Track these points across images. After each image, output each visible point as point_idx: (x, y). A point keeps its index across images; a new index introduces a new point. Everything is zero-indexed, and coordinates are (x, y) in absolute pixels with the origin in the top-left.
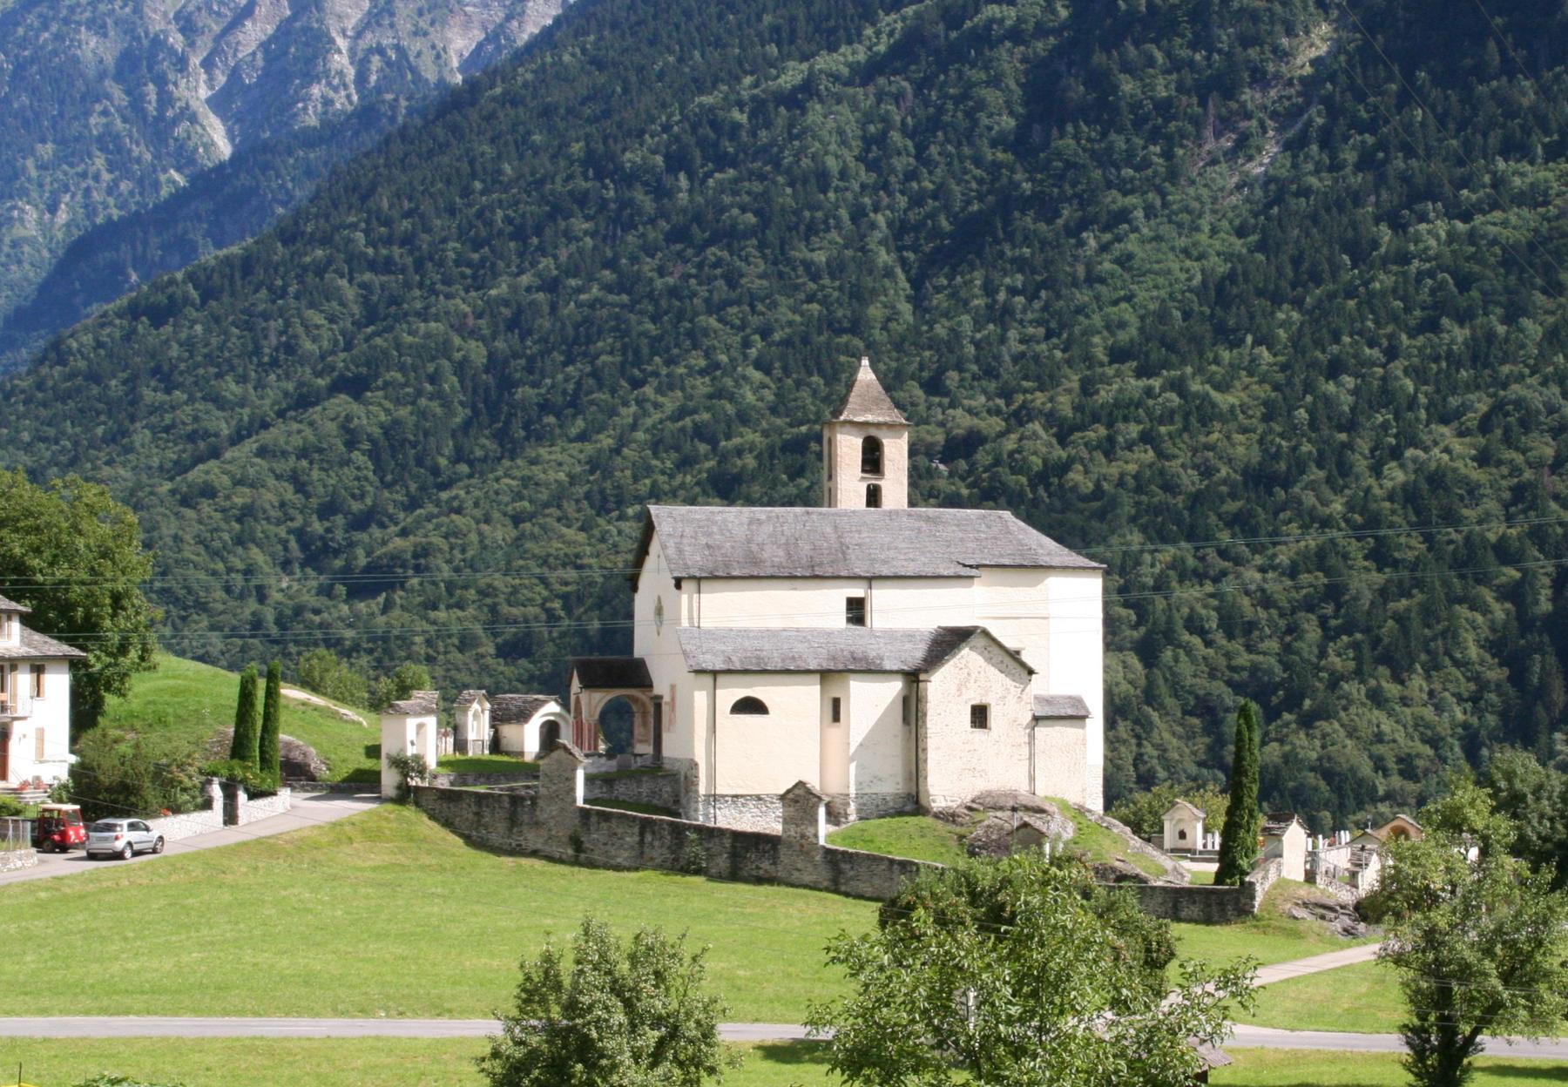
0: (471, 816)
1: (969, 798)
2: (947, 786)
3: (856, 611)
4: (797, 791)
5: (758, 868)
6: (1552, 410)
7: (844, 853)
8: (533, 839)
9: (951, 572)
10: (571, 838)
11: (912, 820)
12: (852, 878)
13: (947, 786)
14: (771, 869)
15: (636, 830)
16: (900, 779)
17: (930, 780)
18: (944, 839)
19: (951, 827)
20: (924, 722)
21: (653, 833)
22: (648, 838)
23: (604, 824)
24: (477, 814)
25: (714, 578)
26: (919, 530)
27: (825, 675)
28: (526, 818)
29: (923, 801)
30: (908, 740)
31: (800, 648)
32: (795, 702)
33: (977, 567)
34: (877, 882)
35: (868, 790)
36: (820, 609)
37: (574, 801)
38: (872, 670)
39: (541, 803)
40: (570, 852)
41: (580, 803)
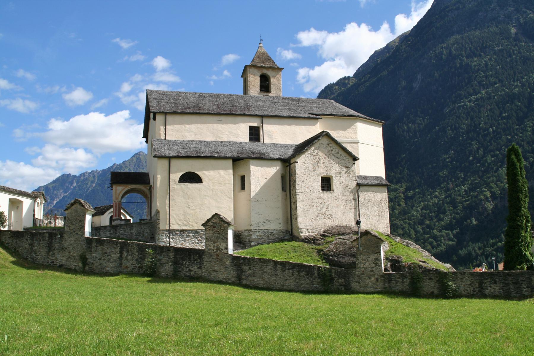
0: (27, 246)
1: (322, 230)
2: (308, 223)
3: (255, 134)
4: (214, 220)
5: (190, 271)
6: (401, 225)
7: (245, 258)
8: (60, 258)
9: (306, 116)
10: (81, 256)
11: (289, 245)
12: (249, 275)
13: (308, 223)
14: (199, 271)
15: (118, 250)
16: (281, 221)
17: (299, 220)
18: (309, 252)
19: (314, 246)
20: (295, 187)
21: (128, 251)
22: (125, 254)
23: (100, 248)
24: (31, 245)
25: (174, 113)
26: (288, 103)
27: (237, 161)
28: (57, 246)
29: (295, 233)
30: (286, 199)
31: (220, 148)
32: (218, 179)
33: (320, 115)
34: (266, 276)
35: (262, 228)
36: (236, 132)
37: (84, 234)
38: (263, 158)
39: (65, 236)
40: (80, 265)
41: (87, 235)
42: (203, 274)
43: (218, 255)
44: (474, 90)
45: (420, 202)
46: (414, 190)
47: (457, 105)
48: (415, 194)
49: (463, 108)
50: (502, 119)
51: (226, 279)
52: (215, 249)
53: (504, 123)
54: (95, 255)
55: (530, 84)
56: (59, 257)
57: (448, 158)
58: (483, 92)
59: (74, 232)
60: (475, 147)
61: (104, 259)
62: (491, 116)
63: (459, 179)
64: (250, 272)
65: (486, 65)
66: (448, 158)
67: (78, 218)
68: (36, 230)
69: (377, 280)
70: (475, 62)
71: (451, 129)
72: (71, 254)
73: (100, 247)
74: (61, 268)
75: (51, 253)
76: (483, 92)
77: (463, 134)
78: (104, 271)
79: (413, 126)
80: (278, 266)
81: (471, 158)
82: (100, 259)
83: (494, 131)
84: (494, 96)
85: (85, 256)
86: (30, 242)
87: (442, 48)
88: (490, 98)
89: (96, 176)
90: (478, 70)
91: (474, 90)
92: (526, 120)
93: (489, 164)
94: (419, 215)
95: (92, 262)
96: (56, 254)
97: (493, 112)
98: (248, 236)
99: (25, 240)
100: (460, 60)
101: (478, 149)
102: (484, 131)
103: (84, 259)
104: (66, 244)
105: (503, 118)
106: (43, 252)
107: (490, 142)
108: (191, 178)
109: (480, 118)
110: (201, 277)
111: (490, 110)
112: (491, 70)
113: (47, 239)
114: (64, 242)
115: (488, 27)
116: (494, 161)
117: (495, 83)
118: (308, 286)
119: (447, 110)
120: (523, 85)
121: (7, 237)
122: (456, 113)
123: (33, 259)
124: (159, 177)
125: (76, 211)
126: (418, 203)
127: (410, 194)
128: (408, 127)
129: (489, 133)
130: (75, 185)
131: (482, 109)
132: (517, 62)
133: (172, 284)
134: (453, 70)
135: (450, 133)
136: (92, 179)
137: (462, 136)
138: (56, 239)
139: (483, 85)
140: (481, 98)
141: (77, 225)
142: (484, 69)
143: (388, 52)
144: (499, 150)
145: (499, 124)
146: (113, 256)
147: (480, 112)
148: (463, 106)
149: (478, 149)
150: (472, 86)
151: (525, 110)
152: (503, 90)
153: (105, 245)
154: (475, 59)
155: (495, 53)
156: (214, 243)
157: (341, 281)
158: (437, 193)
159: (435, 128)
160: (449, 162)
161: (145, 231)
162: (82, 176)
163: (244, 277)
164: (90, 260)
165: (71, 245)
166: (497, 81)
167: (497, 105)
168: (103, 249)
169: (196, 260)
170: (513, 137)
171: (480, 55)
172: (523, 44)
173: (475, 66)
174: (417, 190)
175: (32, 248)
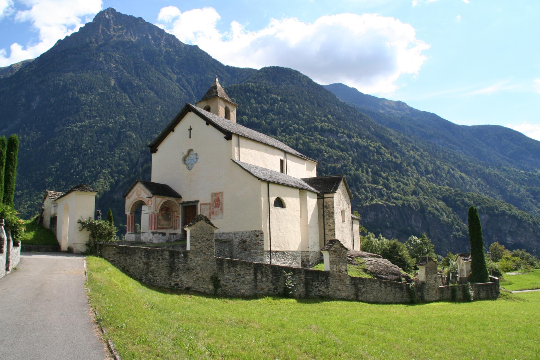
0: (142, 265)
5: (319, 291)
8: (186, 280)
10: (212, 278)
12: (364, 293)
15: (252, 271)
21: (262, 273)
22: (259, 276)
34: (375, 293)
40: (211, 287)
42: (330, 293)
43: (340, 276)
44: (80, 118)
45: (27, 201)
46: (22, 190)
47: (65, 127)
48: (23, 194)
49: (70, 131)
50: (98, 145)
51: (347, 296)
52: (338, 271)
53: (99, 148)
54: (227, 276)
55: (120, 122)
56: (183, 278)
57: (54, 168)
58: (87, 121)
59: (201, 251)
60: (76, 162)
61: (238, 281)
62: (91, 141)
63: (61, 186)
64: (364, 290)
65: (91, 102)
66: (54, 168)
67: (205, 236)
68: (122, 244)
69: (437, 292)
70: (83, 98)
71: (59, 146)
72: (200, 275)
73: (232, 268)
75: (173, 274)
76: (87, 121)
77: (68, 151)
78: (239, 293)
79: (28, 138)
80: (382, 284)
81: (72, 171)
82: (233, 281)
83: (92, 153)
84: (94, 126)
85: (217, 278)
86: (145, 260)
87: (60, 80)
88: (91, 127)
90: (85, 104)
91: (80, 118)
92: (115, 149)
93: (86, 177)
94: (25, 212)
95: (225, 284)
96: (180, 275)
97: (93, 138)
98: (306, 256)
99: (137, 258)
100: (73, 93)
101: (78, 165)
102: (85, 151)
103: (215, 281)
104: (192, 265)
105: (100, 144)
106: (164, 273)
107: (88, 160)
108: (279, 203)
109: (83, 141)
110: (328, 295)
111: (90, 136)
112: (95, 106)
113: (168, 257)
114: (189, 262)
115: (96, 73)
116: (90, 176)
117: (96, 117)
118: (400, 299)
119: (57, 130)
120: (115, 122)
121: (111, 253)
122: (64, 133)
123: (149, 280)
124: (262, 199)
125: (202, 228)
126: (25, 202)
127: (18, 193)
128: (23, 138)
129: (88, 154)
131: (85, 134)
132: (113, 104)
133: (235, 300)
134: (66, 99)
135: (58, 148)
137: (67, 153)
138: (179, 258)
139: (87, 116)
140: (85, 126)
141: (204, 244)
142: (90, 104)
143: (12, 72)
144: (95, 168)
145: (96, 148)
146: (247, 277)
147: (83, 136)
148: (70, 129)
149: (78, 165)
150: (79, 115)
151: (115, 141)
152: (101, 123)
153: (238, 266)
154: (84, 95)
155: (98, 94)
156: (337, 266)
157: (419, 294)
158: (42, 195)
159: (46, 142)
160: (54, 171)
161: (225, 250)
163: (360, 294)
164: (222, 282)
165: (199, 265)
166: (98, 115)
167: (96, 134)
168: (236, 271)
169: (323, 281)
170: (105, 159)
171: (88, 93)
172: (118, 93)
173: (83, 100)
174: (25, 191)
175: (148, 268)
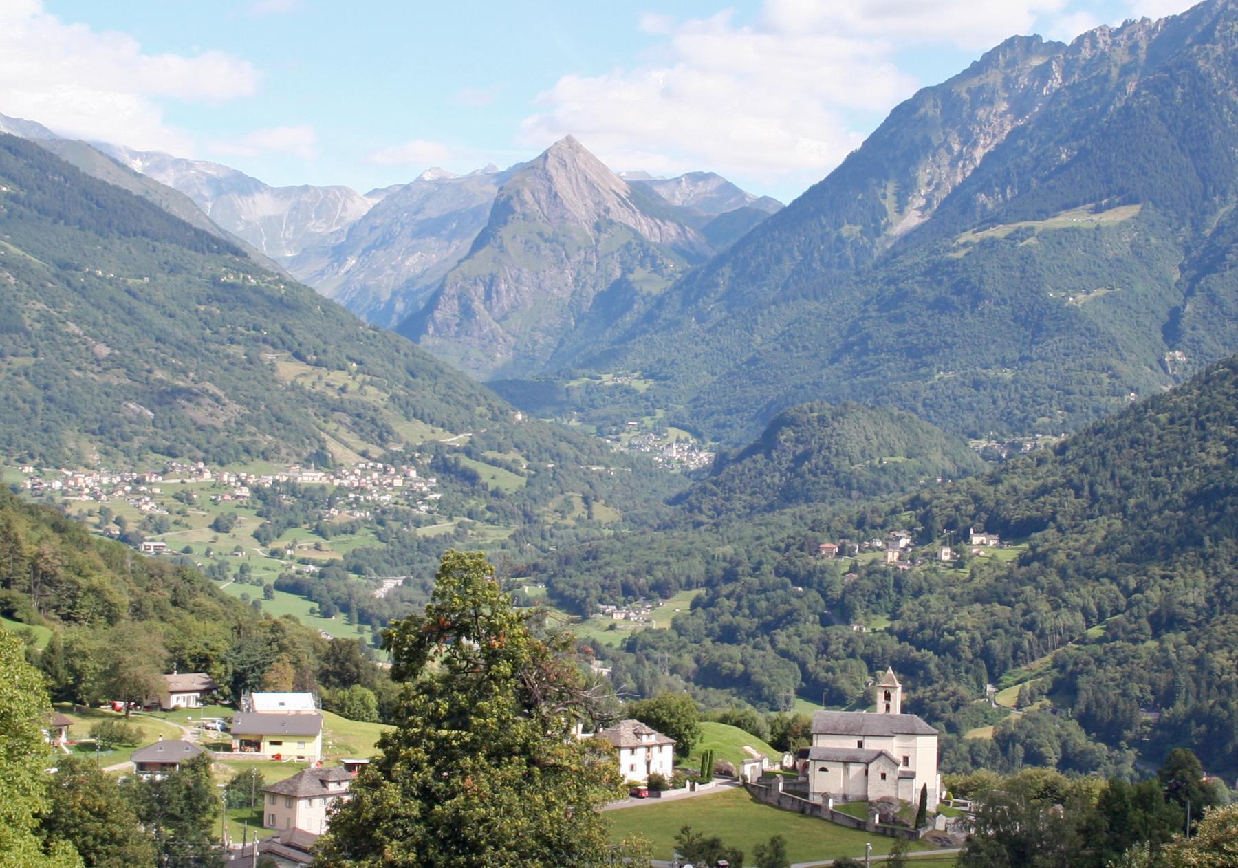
3: (860, 744)
8: (770, 800)
36: (851, 744)
74: (767, 803)
89: (1143, 44)
108: (823, 769)
130: (1056, 82)
136: (1126, 59)
162: (1087, 43)
